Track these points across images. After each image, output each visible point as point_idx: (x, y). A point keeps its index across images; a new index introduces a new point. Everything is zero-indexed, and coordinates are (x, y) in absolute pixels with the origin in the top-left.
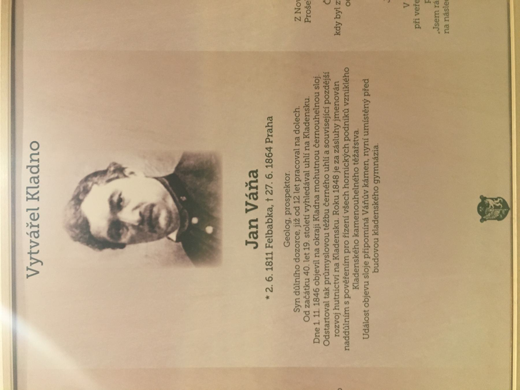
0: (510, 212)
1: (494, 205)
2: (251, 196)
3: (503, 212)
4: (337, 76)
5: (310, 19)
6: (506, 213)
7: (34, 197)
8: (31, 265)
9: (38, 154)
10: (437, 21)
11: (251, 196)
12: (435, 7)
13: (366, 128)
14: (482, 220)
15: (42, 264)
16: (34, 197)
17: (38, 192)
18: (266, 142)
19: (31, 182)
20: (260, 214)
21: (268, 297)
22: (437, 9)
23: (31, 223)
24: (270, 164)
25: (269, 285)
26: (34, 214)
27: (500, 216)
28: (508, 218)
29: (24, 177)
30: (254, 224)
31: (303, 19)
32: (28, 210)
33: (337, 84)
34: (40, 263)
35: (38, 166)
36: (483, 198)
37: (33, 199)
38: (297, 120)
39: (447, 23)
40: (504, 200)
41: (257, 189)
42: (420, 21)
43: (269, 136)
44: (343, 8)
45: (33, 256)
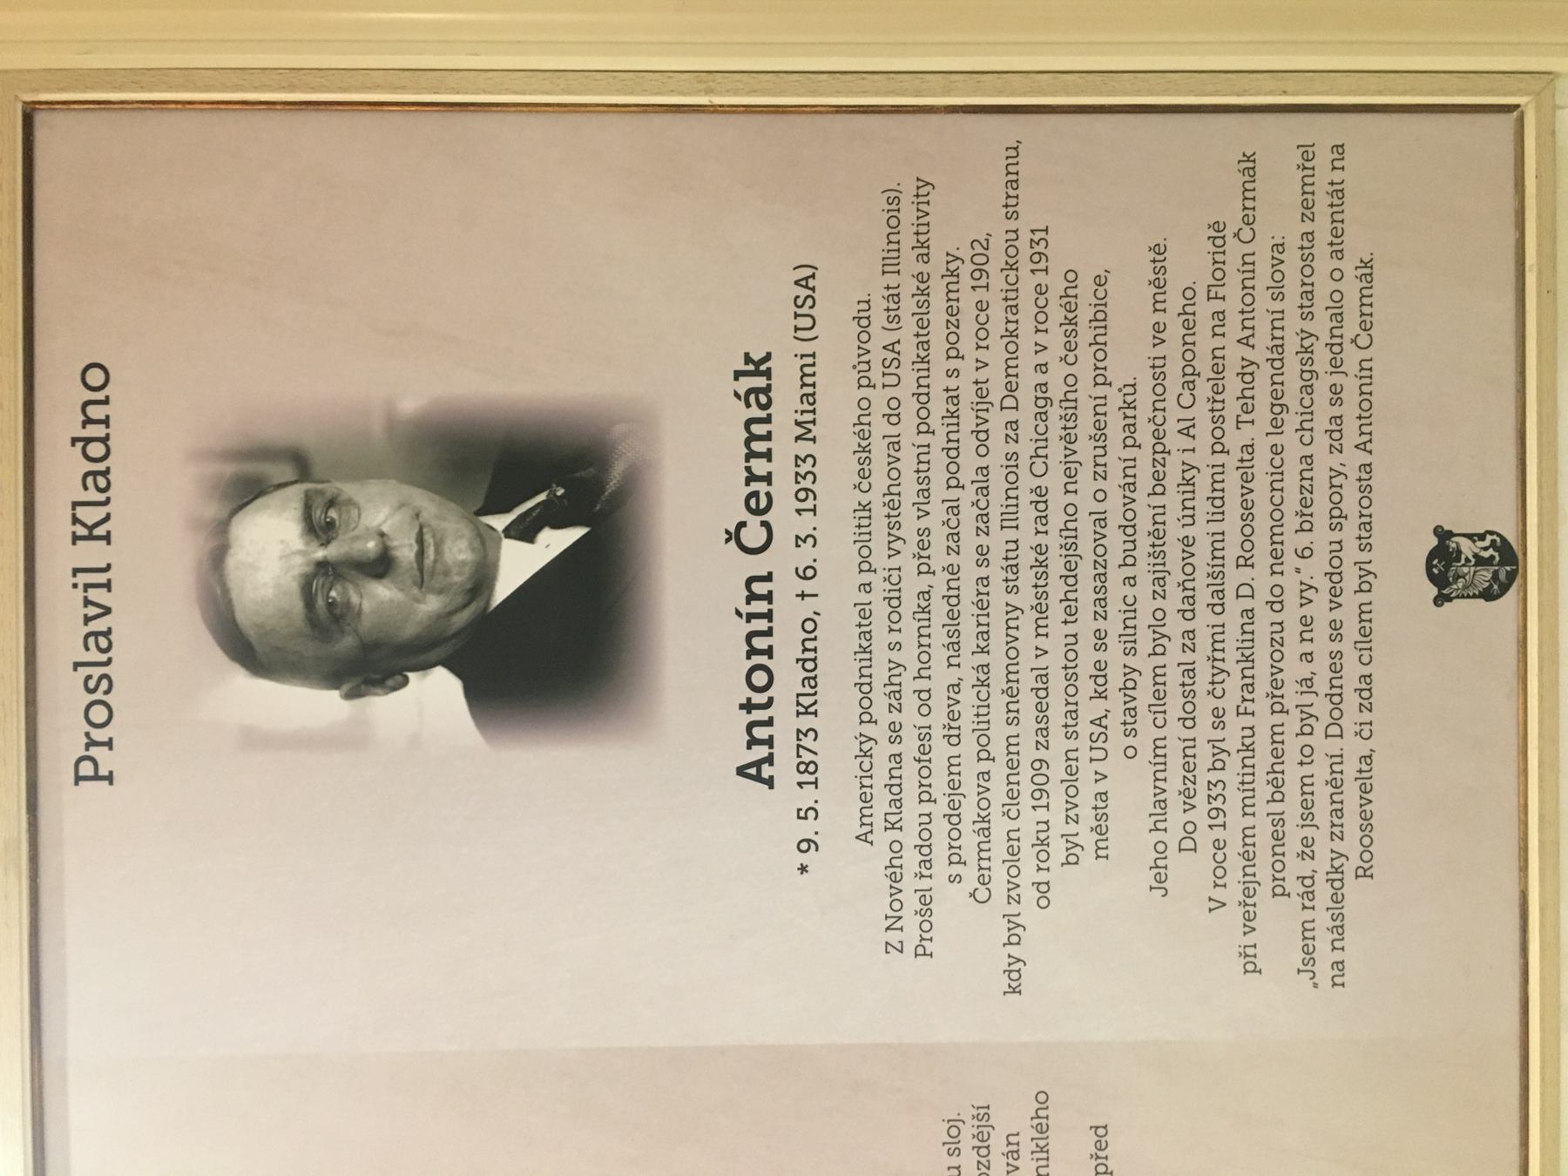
1: (1475, 556)
2: (752, 398)
3: (1502, 576)
4: (1012, 1118)
5: (929, 946)
6: (1512, 577)
7: (97, 532)
9: (106, 401)
10: (1309, 953)
11: (752, 398)
12: (1304, 907)
14: (1440, 600)
16: (97, 532)
17: (107, 518)
19: (86, 488)
21: (803, 869)
22: (1308, 915)
23: (87, 735)
24: (811, 778)
25: (806, 829)
28: (1512, 593)
29: (62, 473)
30: (760, 588)
31: (909, 949)
33: (1012, 1139)
35: (107, 437)
36: (1443, 535)
37: (90, 537)
38: (894, 230)
39: (1338, 956)
40: (1503, 539)
41: (770, 620)
42: (1258, 951)
44: (1028, 912)
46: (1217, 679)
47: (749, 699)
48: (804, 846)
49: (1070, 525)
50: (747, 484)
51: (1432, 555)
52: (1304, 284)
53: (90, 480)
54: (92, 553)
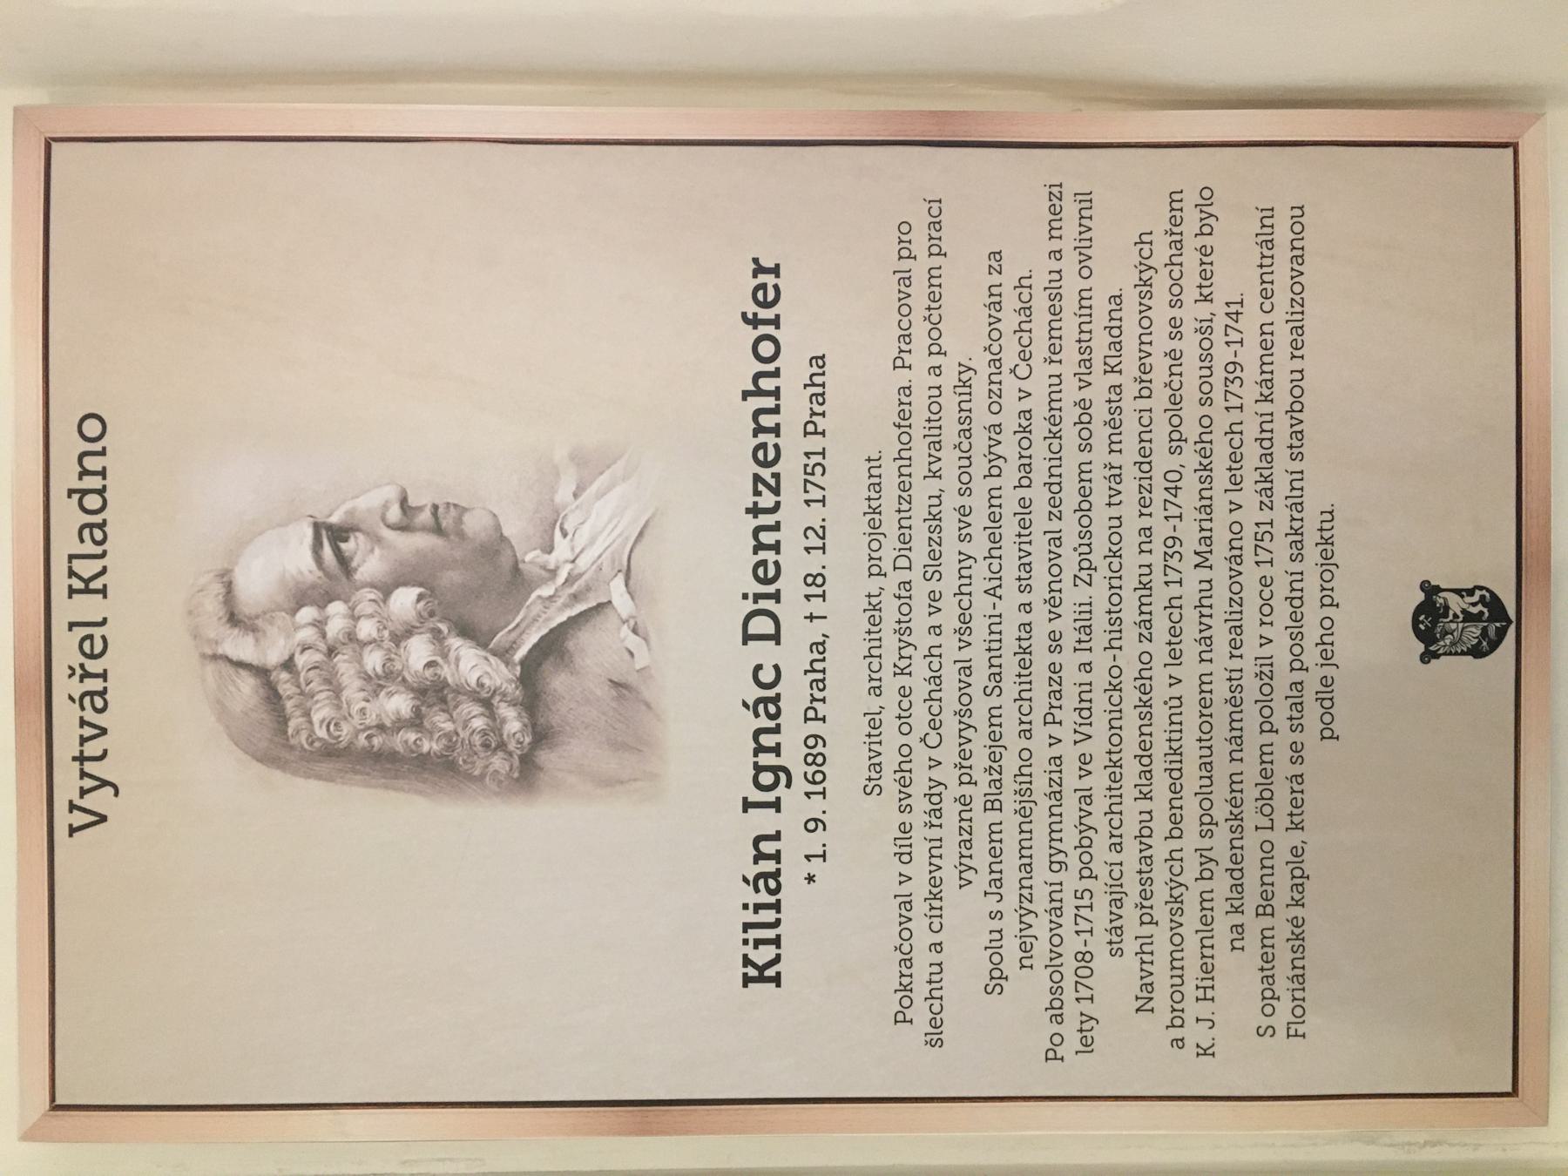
0: (1512, 630)
1: (1464, 611)
2: (761, 883)
6: (1501, 634)
7: (92, 585)
8: (82, 797)
9: (103, 453)
11: (761, 883)
13: (1176, 964)
14: (1427, 657)
15: (116, 794)
16: (92, 585)
17: (104, 571)
18: (806, 434)
19: (82, 541)
20: (792, 656)
23: (82, 666)
24: (819, 591)
26: (91, 637)
27: (1480, 643)
30: (767, 847)
32: (72, 625)
34: (109, 790)
36: (1430, 590)
37: (87, 591)
41: (778, 862)
43: (813, 414)
45: (89, 767)
46: (1085, 1026)
47: (755, 503)
48: (811, 825)
49: (1025, 770)
50: (755, 553)
51: (1419, 610)
52: (1112, 836)
53: (86, 532)
54: (88, 608)
